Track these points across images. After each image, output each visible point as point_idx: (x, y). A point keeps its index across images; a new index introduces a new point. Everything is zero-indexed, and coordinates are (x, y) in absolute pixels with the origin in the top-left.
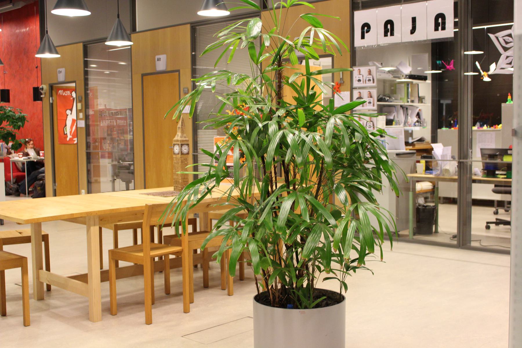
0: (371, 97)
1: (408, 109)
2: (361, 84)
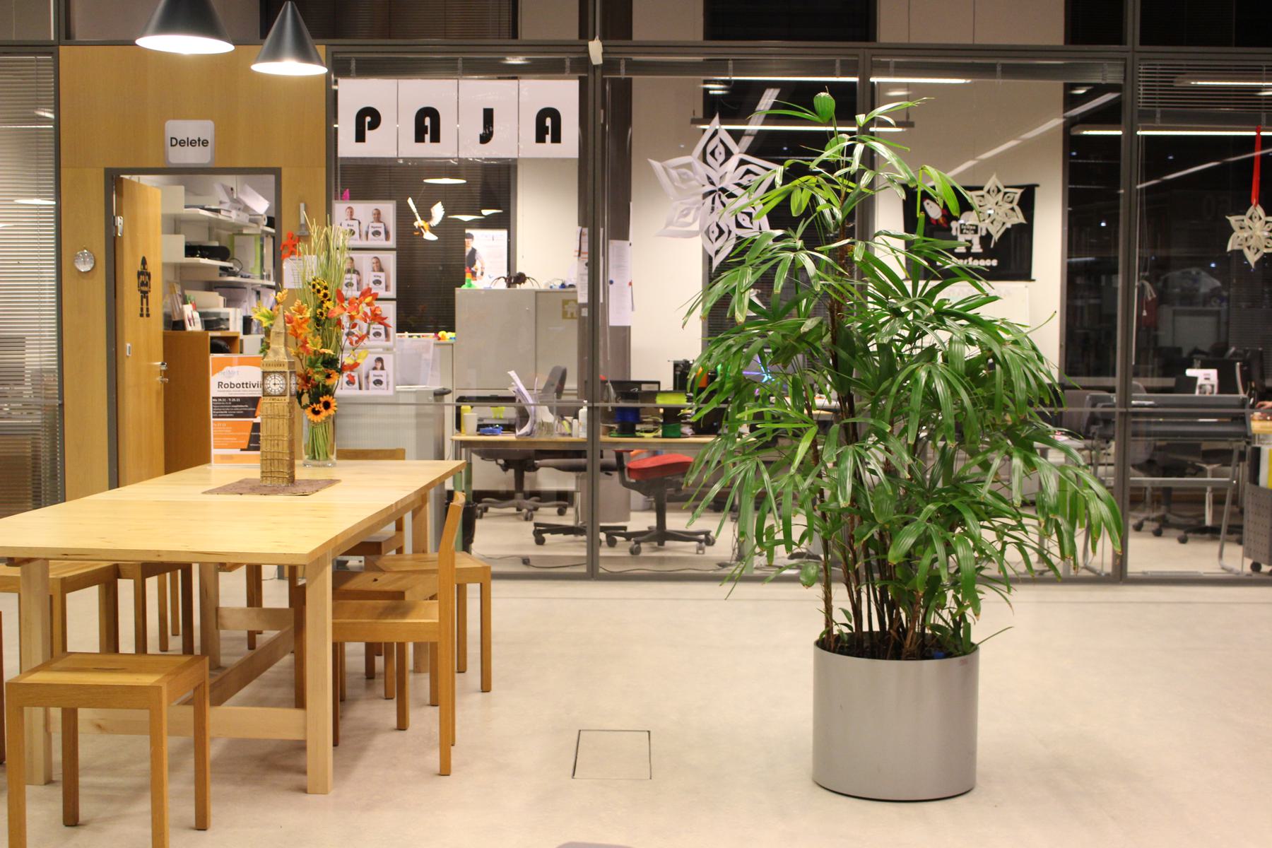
0: (381, 270)
1: (262, 293)
2: (356, 240)
